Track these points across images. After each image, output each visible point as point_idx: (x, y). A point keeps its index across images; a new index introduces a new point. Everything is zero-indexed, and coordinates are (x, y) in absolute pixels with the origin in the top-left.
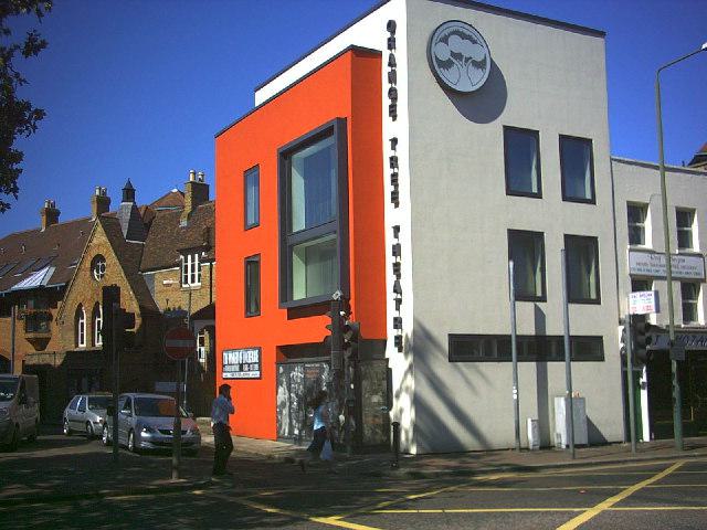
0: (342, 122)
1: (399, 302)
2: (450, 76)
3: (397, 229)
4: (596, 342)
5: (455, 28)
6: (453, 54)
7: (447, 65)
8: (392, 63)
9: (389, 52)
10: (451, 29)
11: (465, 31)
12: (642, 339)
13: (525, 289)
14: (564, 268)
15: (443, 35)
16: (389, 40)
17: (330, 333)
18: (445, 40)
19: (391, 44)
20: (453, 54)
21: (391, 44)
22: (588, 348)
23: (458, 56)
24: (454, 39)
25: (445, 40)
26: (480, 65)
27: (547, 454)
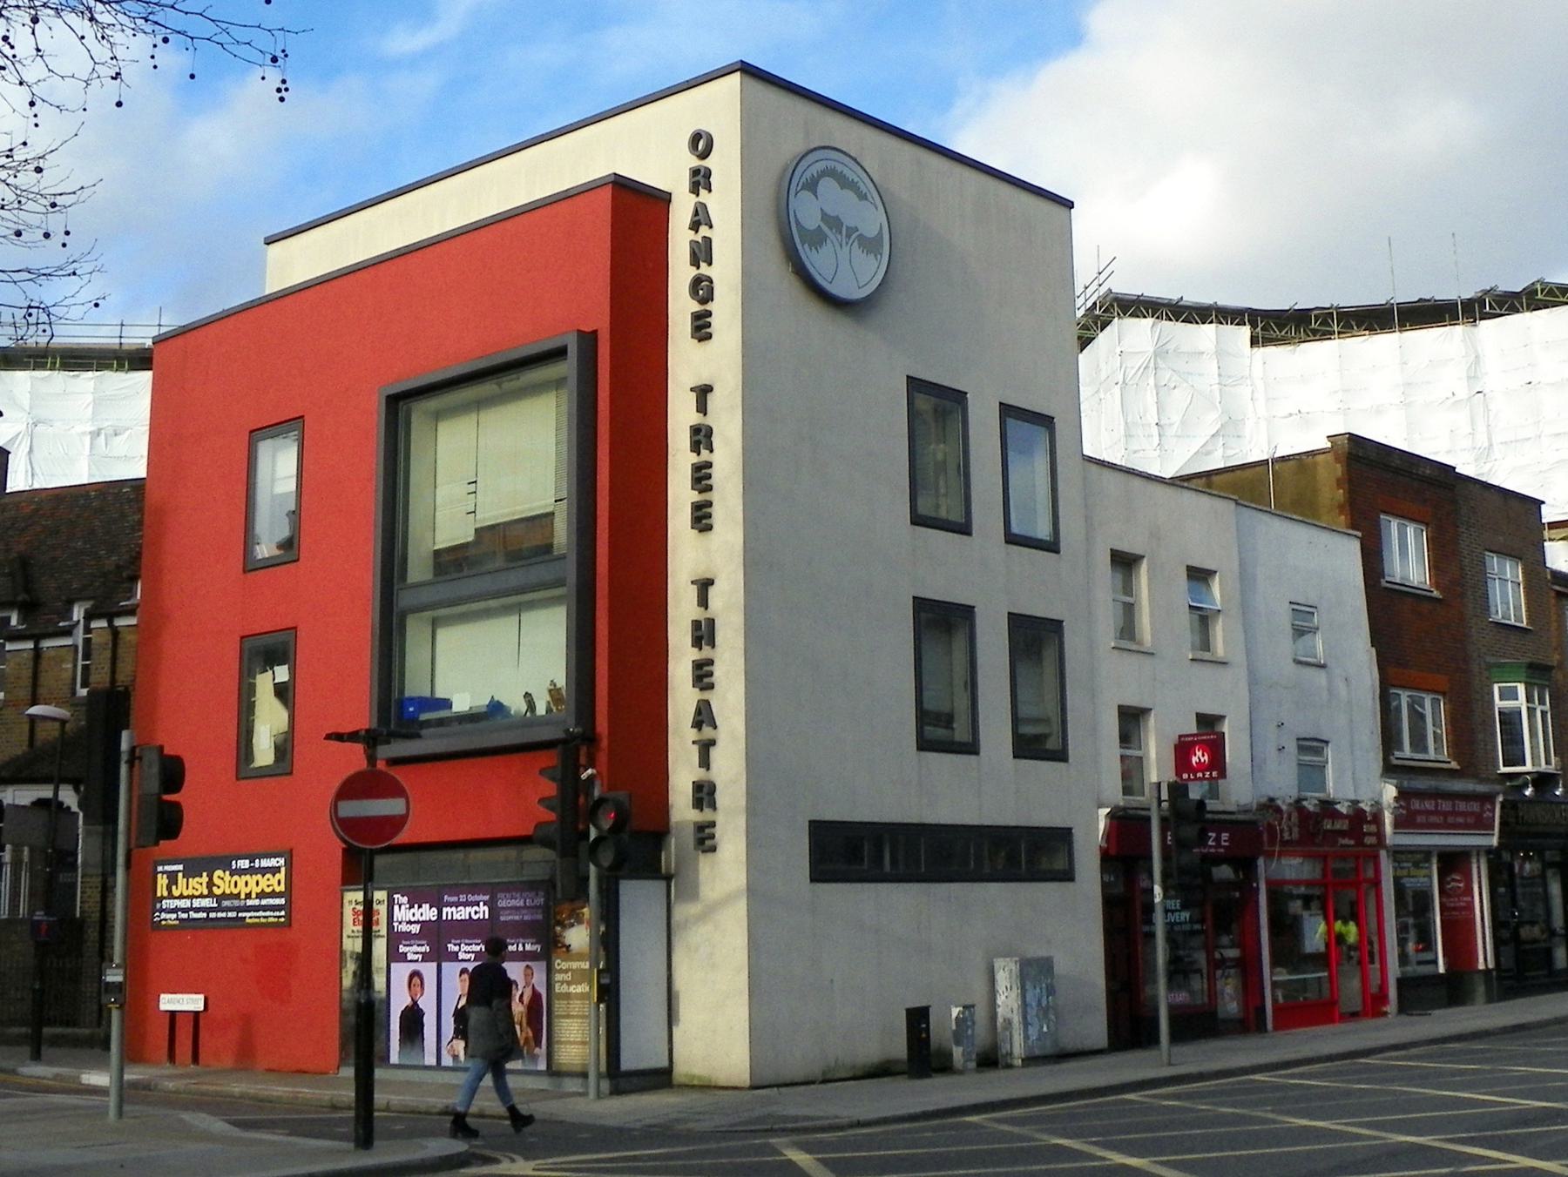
0: (589, 340)
1: (706, 747)
2: (820, 262)
3: (704, 586)
4: (1062, 837)
5: (830, 164)
6: (825, 217)
7: (817, 239)
8: (700, 219)
9: (693, 199)
10: (821, 166)
11: (847, 172)
12: (1190, 831)
13: (942, 731)
14: (24, 787)
15: (808, 175)
16: (695, 172)
17: (552, 816)
18: (812, 186)
19: (700, 180)
20: (825, 217)
21: (700, 180)
22: (1027, 854)
23: (834, 222)
24: (827, 186)
25: (812, 186)
26: (870, 245)
27: (992, 1075)
